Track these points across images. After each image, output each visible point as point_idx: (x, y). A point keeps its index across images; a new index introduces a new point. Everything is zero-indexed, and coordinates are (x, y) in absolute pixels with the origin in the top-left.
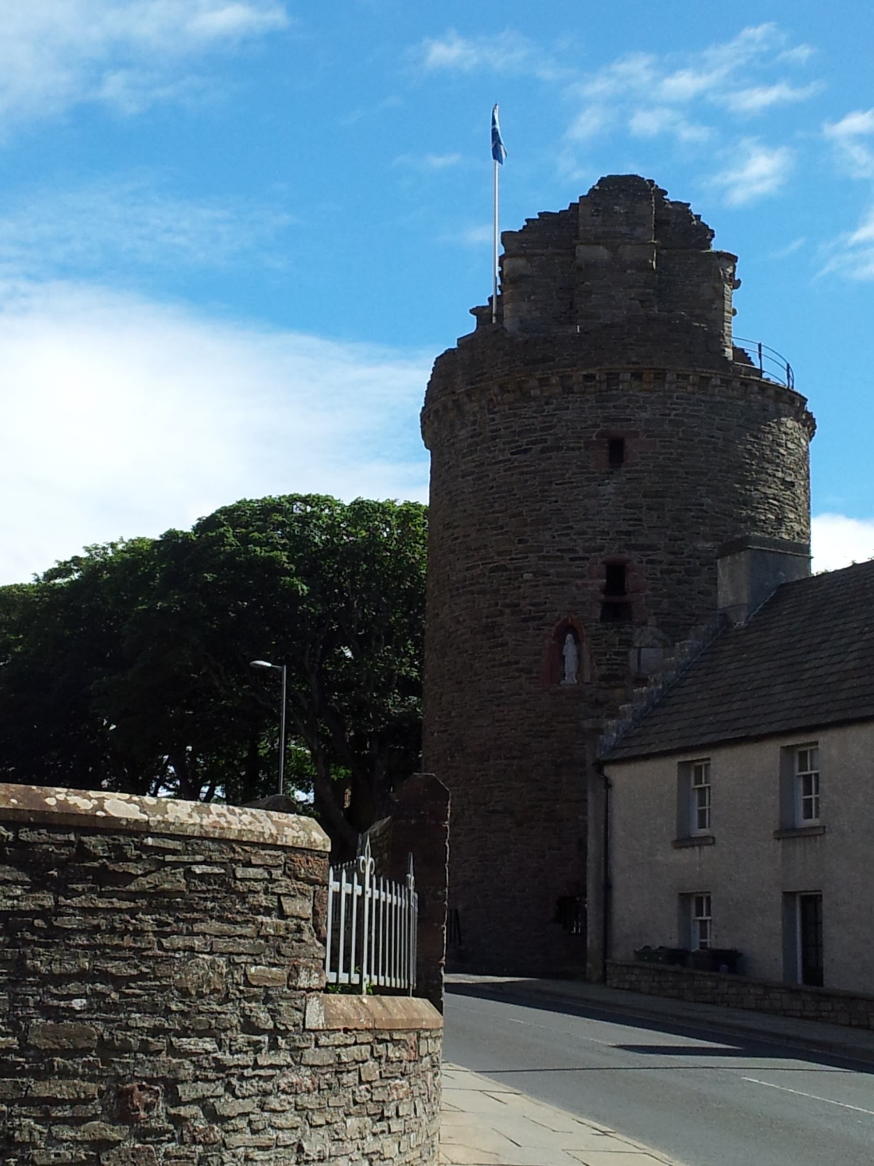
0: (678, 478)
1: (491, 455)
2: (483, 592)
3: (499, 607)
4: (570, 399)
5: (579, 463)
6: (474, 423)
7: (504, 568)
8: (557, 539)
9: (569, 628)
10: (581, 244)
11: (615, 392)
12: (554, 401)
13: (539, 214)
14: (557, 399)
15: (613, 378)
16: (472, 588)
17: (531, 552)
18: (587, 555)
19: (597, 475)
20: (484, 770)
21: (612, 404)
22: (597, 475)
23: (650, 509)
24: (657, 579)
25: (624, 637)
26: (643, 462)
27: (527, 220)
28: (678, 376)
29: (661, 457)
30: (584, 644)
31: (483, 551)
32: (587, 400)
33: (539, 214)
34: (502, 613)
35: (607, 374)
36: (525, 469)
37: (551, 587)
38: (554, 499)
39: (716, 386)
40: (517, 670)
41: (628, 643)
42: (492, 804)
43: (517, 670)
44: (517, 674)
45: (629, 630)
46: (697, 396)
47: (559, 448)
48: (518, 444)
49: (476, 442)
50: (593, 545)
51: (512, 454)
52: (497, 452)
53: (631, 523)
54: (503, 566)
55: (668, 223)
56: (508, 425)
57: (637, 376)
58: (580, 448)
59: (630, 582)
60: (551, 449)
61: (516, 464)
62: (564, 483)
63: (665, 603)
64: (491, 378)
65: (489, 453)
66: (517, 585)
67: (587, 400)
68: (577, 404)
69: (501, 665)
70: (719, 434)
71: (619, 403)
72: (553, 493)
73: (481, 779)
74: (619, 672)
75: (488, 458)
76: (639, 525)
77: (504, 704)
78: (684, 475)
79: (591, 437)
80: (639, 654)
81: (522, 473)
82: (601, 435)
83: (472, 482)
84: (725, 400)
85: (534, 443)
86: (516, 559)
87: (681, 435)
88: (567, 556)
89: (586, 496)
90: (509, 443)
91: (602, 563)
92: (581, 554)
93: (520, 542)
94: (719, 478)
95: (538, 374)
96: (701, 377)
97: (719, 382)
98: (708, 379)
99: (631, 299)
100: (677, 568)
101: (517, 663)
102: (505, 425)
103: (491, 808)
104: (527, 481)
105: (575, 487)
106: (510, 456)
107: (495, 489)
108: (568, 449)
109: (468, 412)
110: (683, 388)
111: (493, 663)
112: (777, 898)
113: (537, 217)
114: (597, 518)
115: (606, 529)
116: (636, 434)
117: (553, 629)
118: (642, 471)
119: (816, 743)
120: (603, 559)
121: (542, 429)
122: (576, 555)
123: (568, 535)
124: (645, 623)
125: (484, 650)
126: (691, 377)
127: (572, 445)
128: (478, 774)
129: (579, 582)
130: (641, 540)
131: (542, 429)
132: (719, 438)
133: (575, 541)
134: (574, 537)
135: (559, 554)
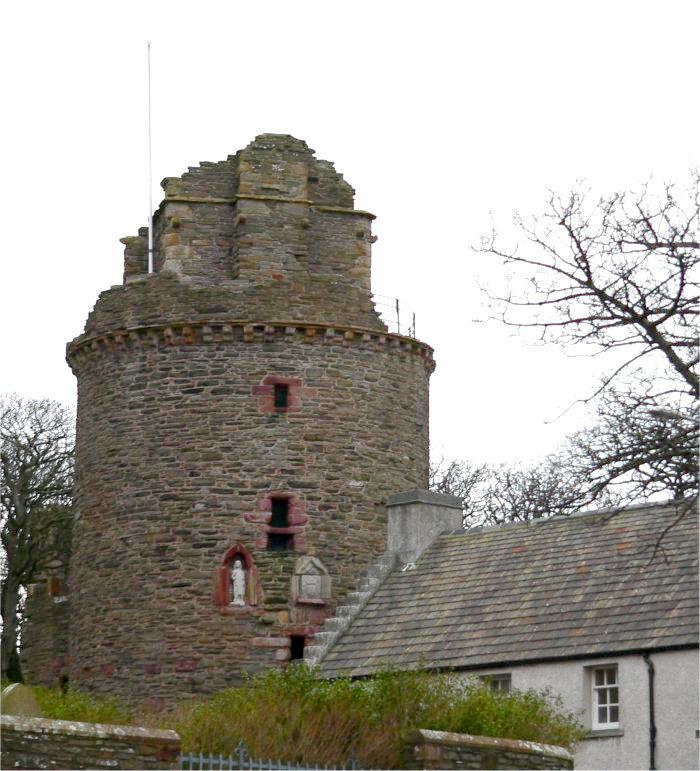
1: (161, 392)
13: (201, 163)
21: (277, 354)
28: (336, 332)
32: (256, 349)
33: (201, 163)
38: (224, 437)
41: (290, 570)
43: (189, 592)
47: (228, 391)
51: (184, 392)
56: (180, 365)
59: (293, 516)
68: (247, 352)
70: (367, 384)
79: (258, 383)
80: (300, 581)
81: (193, 412)
82: (268, 381)
88: (237, 491)
92: (249, 489)
93: (192, 475)
100: (332, 505)
104: (199, 419)
106: (181, 394)
116: (298, 382)
118: (304, 417)
119: (509, 675)
121: (213, 373)
124: (304, 553)
126: (347, 333)
127: (241, 389)
129: (248, 514)
130: (303, 479)
131: (213, 373)
134: (244, 473)
135: (229, 488)
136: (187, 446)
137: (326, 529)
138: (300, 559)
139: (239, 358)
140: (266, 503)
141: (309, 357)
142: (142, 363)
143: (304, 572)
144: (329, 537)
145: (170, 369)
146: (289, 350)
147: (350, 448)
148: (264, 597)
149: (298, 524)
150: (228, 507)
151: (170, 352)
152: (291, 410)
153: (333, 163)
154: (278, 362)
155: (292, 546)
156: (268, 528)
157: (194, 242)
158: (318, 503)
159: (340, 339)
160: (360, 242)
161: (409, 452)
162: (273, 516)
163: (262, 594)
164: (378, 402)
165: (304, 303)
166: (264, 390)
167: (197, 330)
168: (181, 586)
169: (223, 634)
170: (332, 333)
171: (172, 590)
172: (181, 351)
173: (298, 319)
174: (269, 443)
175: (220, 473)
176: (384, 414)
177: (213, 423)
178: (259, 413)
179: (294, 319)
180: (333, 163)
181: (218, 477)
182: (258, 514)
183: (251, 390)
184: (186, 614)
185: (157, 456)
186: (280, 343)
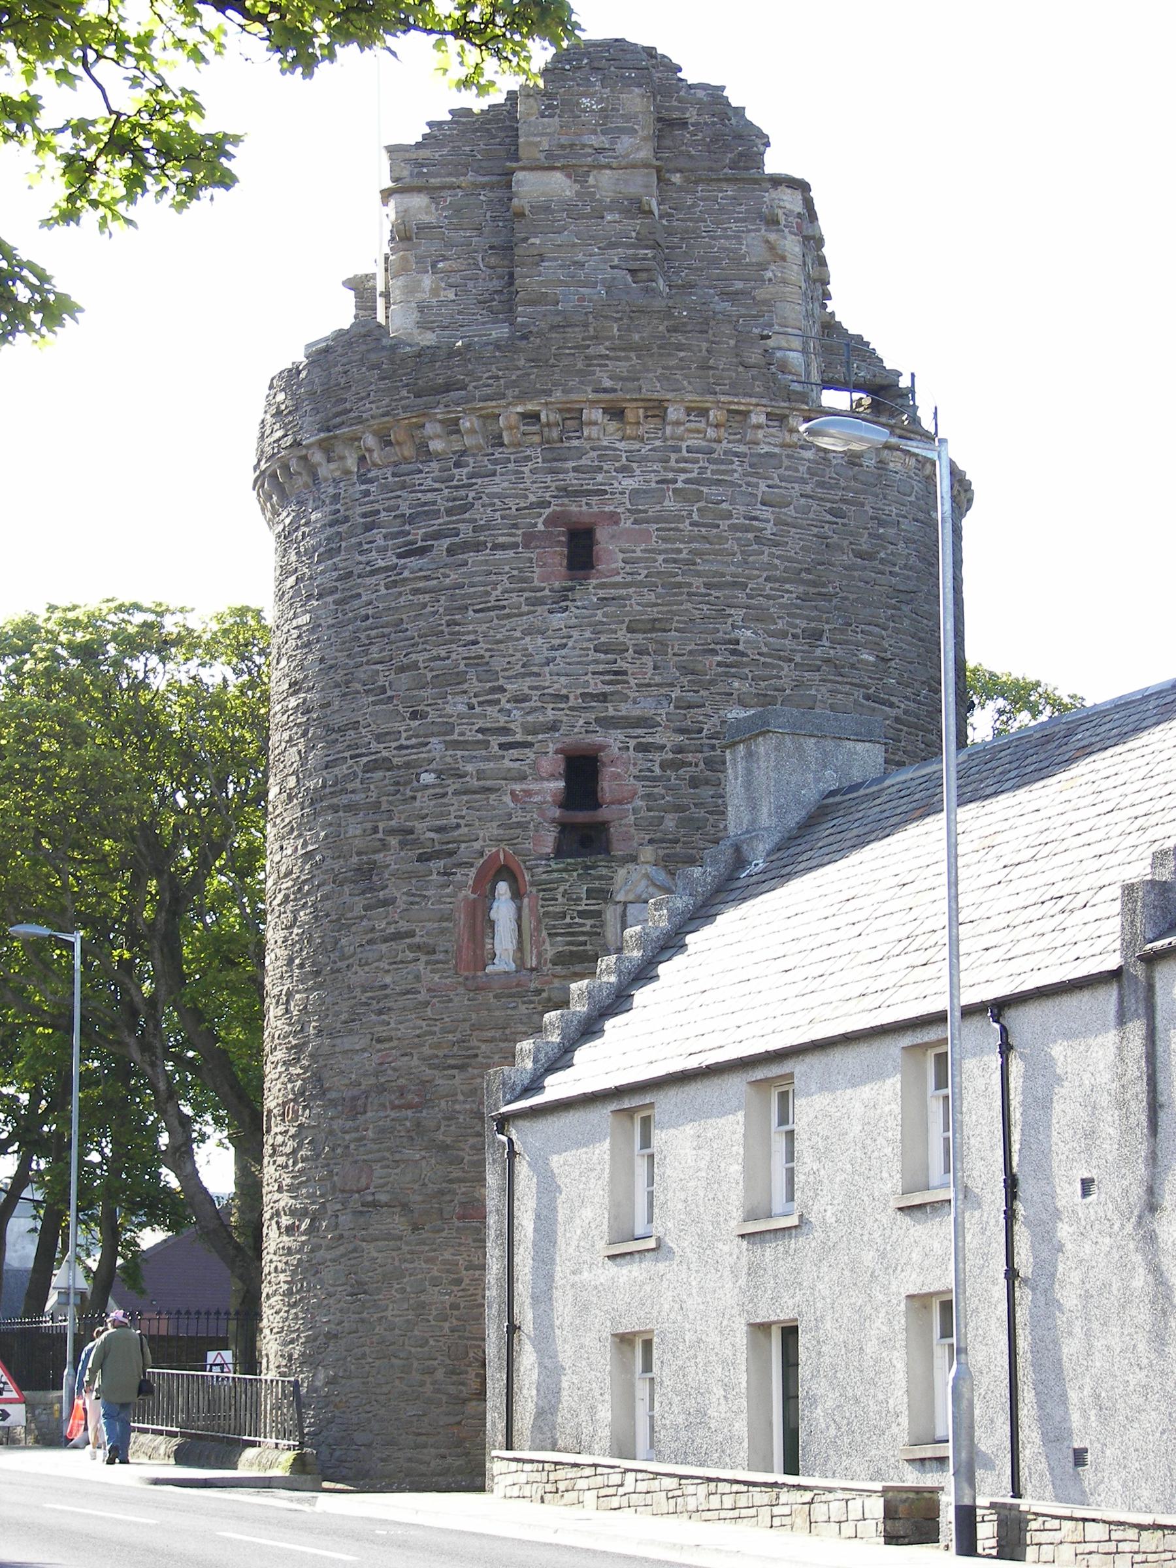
0: (689, 594)
1: (363, 559)
2: (350, 808)
3: (380, 835)
4: (497, 456)
5: (515, 573)
6: (336, 498)
7: (384, 764)
8: (478, 710)
9: (506, 872)
10: (523, 169)
11: (576, 443)
12: (471, 460)
13: (451, 112)
14: (474, 455)
15: (573, 416)
16: (335, 800)
17: (433, 735)
18: (529, 738)
19: (547, 592)
20: (357, 1130)
21: (570, 464)
22: (547, 592)
23: (641, 652)
24: (654, 779)
25: (597, 884)
26: (628, 570)
27: (430, 124)
28: (689, 411)
29: (661, 558)
30: (526, 900)
31: (351, 732)
32: (528, 458)
33: (451, 112)
34: (385, 846)
35: (560, 410)
36: (421, 584)
37: (465, 798)
38: (471, 637)
39: (759, 427)
40: (411, 947)
41: (603, 895)
42: (372, 1190)
43: (411, 947)
44: (411, 956)
45: (604, 872)
46: (724, 444)
47: (478, 547)
48: (410, 537)
49: (339, 533)
50: (541, 719)
51: (400, 556)
52: (374, 553)
53: (607, 678)
54: (386, 759)
55: (684, 124)
56: (392, 502)
57: (616, 413)
58: (515, 546)
59: (607, 786)
60: (466, 547)
61: (406, 574)
62: (488, 609)
63: (670, 821)
64: (360, 420)
65: (361, 553)
66: (409, 793)
67: (528, 458)
68: (511, 466)
69: (386, 940)
70: (767, 513)
71: (583, 462)
72: (471, 628)
73: (352, 1146)
74: (588, 947)
75: (360, 563)
76: (618, 682)
77: (389, 1009)
78: (703, 590)
79: (535, 525)
80: (624, 911)
81: (415, 592)
82: (551, 521)
83: (333, 607)
84: (777, 450)
85: (437, 535)
86: (407, 747)
87: (695, 516)
88: (495, 741)
89: (526, 632)
90: (394, 536)
91: (557, 752)
92: (519, 737)
93: (414, 715)
94: (768, 592)
95: (439, 412)
96: (729, 411)
97: (762, 419)
98: (745, 414)
99: (612, 267)
100: (690, 757)
101: (411, 934)
102: (387, 504)
103: (370, 1198)
104: (425, 606)
105: (509, 616)
106: (395, 561)
107: (371, 620)
108: (496, 547)
109: (326, 480)
110: (698, 432)
111: (370, 936)
112: (741, 1338)
113: (449, 118)
114: (547, 669)
115: (564, 692)
116: (614, 518)
117: (473, 873)
118: (626, 585)
119: (791, 1075)
120: (559, 746)
121: (449, 512)
122: (510, 739)
123: (498, 702)
124: (633, 859)
125: (355, 914)
126: (711, 413)
127: (501, 540)
128: (347, 1137)
129: (517, 787)
130: (625, 709)
131: (449, 512)
132: (768, 521)
133: (509, 712)
134: (508, 706)
135: (480, 737)
136: (405, 661)
137: (679, 808)
138: (622, 872)
139: (497, 479)
140: (552, 763)
141: (635, 465)
142: (334, 507)
143: (631, 897)
144: (681, 823)
145: (378, 512)
146: (594, 454)
147: (730, 642)
148: (550, 952)
149: (620, 802)
150: (481, 775)
151: (376, 479)
152: (602, 574)
153: (723, 88)
154: (572, 479)
155: (606, 849)
156: (557, 813)
157: (441, 265)
158: (657, 757)
159: (703, 425)
160: (772, 237)
161: (875, 646)
162: (567, 787)
163: (547, 946)
164: (793, 548)
165: (618, 359)
166: (546, 535)
167: (417, 433)
168: (397, 936)
169: (474, 1028)
170: (682, 416)
171: (384, 947)
172: (394, 475)
173: (605, 391)
174: (557, 642)
175: (462, 708)
176: (808, 571)
177: (449, 611)
178: (536, 583)
179: (595, 391)
180: (723, 88)
181: (460, 716)
182: (535, 787)
183: (519, 539)
184: (408, 992)
185: (358, 686)
186: (576, 443)
